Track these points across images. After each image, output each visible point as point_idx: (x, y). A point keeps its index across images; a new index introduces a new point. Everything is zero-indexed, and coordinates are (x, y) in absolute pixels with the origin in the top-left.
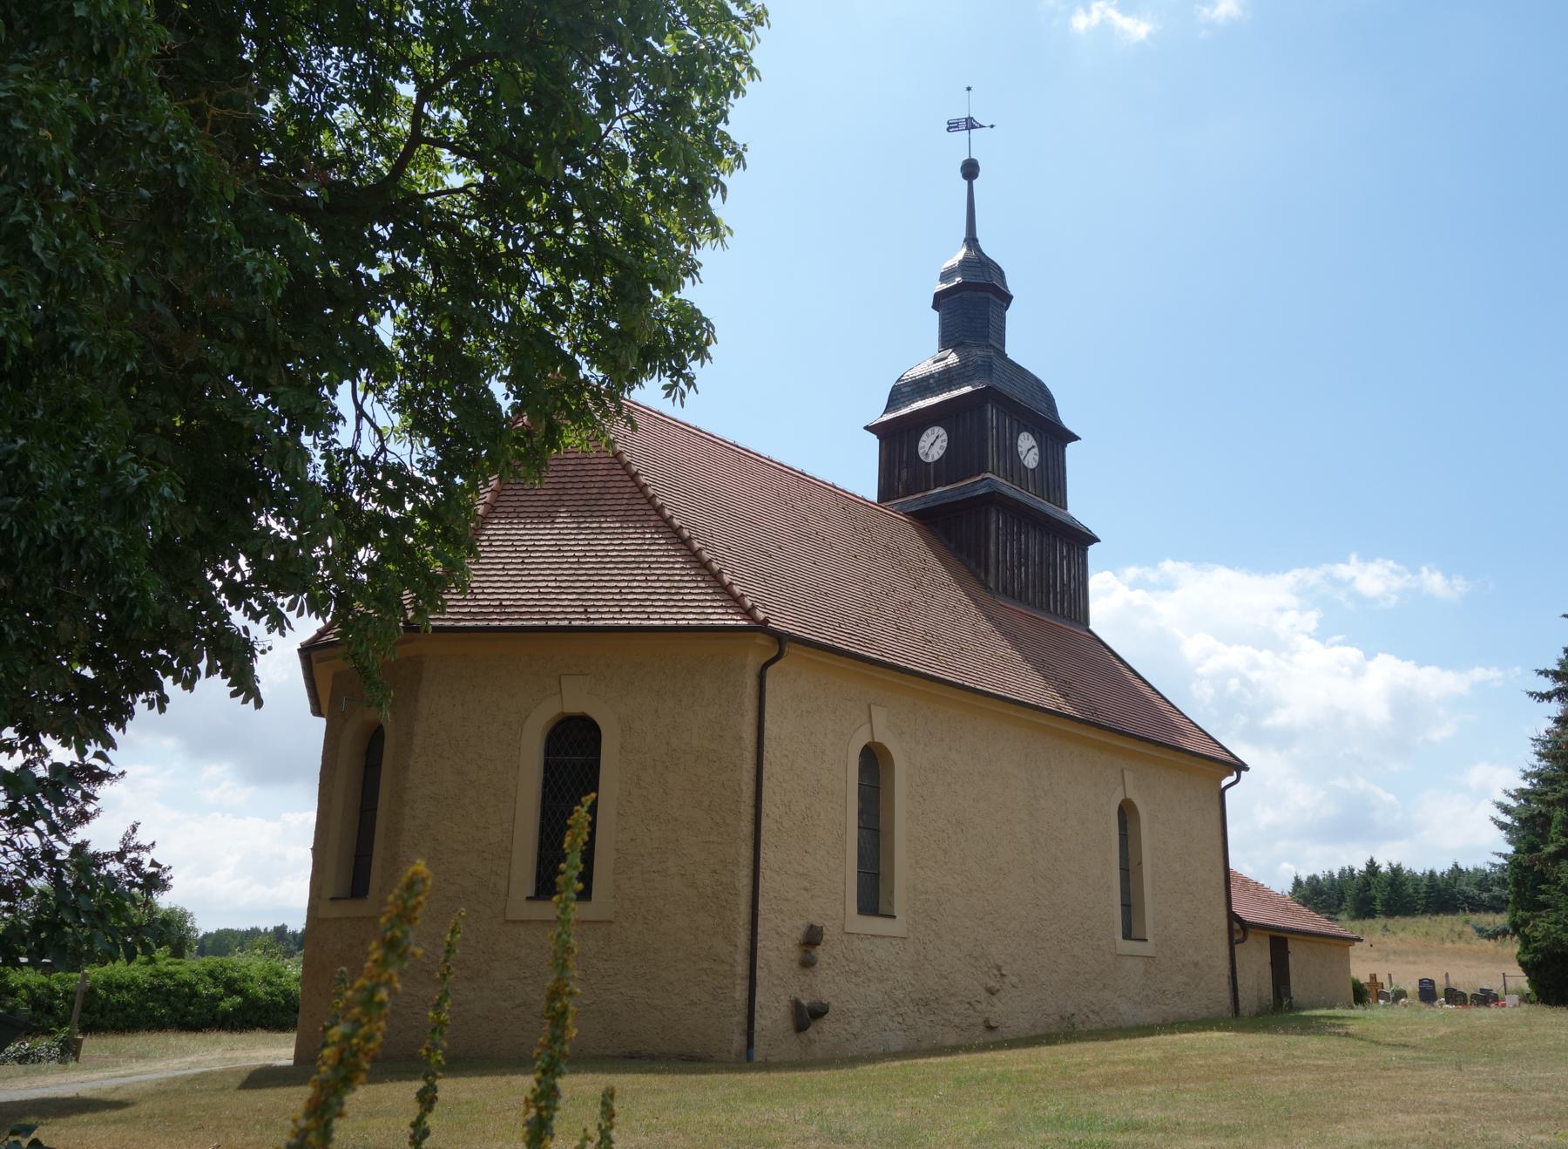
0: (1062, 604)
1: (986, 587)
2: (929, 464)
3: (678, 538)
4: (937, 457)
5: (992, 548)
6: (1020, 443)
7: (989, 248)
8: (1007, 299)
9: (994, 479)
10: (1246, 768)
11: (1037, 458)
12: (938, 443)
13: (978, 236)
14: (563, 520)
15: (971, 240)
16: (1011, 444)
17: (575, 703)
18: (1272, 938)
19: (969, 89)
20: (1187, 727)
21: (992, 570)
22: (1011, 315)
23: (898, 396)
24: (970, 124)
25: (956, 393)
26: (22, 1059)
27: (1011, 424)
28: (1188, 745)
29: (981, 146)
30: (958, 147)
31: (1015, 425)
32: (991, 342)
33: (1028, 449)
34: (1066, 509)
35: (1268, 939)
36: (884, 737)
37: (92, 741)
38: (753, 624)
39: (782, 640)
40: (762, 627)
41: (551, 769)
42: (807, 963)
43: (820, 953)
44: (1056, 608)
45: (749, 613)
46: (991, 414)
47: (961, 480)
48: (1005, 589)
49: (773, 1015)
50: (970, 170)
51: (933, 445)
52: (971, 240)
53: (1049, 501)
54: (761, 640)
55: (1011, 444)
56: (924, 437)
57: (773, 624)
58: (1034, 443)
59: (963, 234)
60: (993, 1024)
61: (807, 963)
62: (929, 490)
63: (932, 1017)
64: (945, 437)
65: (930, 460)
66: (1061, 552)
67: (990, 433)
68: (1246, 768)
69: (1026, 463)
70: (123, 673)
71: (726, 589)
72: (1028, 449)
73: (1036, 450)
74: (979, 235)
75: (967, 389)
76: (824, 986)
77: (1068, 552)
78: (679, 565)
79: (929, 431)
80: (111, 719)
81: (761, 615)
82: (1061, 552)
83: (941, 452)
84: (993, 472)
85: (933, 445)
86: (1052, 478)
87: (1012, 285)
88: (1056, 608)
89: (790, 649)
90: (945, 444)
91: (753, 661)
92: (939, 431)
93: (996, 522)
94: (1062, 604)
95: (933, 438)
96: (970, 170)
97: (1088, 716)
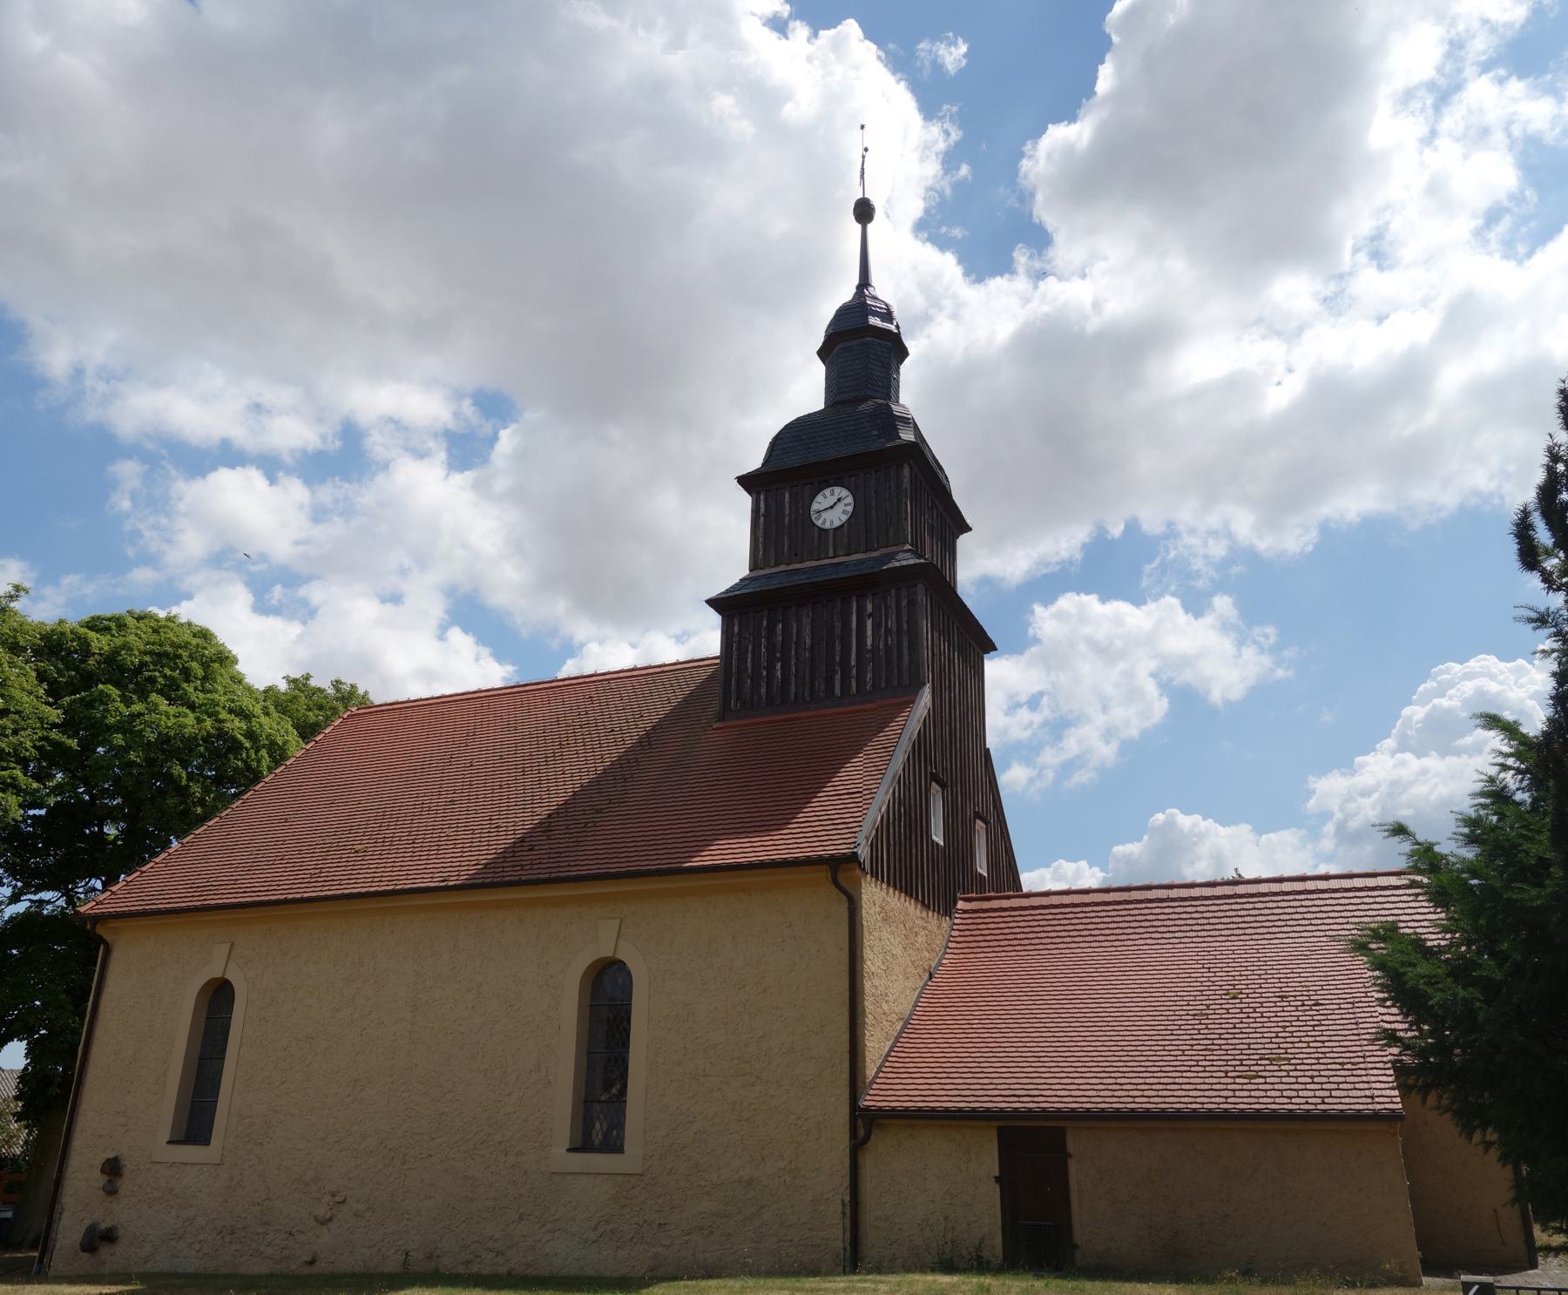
2: (826, 531)
12: (840, 507)
13: (854, 290)
18: (1000, 1129)
26: (1048, 564)
35: (994, 1134)
42: (111, 1191)
43: (124, 1185)
49: (68, 1232)
60: (309, 1259)
61: (111, 1191)
63: (238, 1247)
64: (850, 500)
70: (27, 650)
76: (122, 1213)
79: (827, 492)
80: (930, 235)
83: (845, 518)
90: (850, 509)
95: (833, 500)
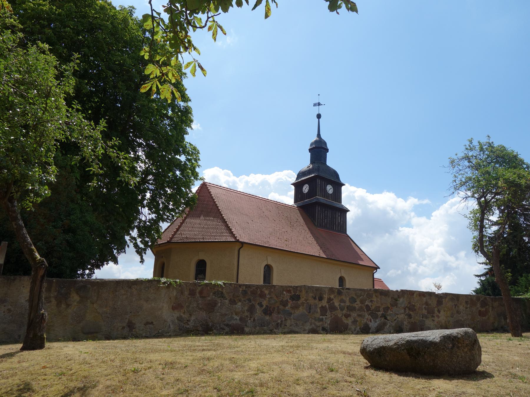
0: (338, 227)
1: (315, 225)
3: (224, 222)
4: (307, 192)
5: (317, 215)
6: (327, 187)
7: (323, 137)
8: (327, 150)
9: (320, 198)
10: (379, 268)
11: (332, 191)
13: (321, 134)
14: (202, 218)
15: (319, 135)
16: (325, 188)
17: (201, 258)
19: (319, 95)
20: (363, 257)
21: (316, 221)
22: (328, 154)
23: (300, 175)
24: (319, 104)
25: (311, 176)
27: (324, 184)
28: (361, 263)
29: (321, 110)
30: (316, 110)
31: (326, 183)
32: (322, 162)
33: (330, 189)
34: (341, 203)
36: (270, 262)
37: (155, 218)
38: (236, 240)
39: (243, 243)
40: (238, 241)
41: (197, 270)
44: (336, 228)
45: (235, 238)
46: (319, 181)
47: (312, 198)
48: (320, 225)
50: (319, 116)
51: (306, 189)
52: (319, 135)
53: (336, 201)
54: (238, 244)
55: (325, 188)
56: (304, 187)
57: (241, 240)
58: (332, 187)
59: (317, 133)
62: (305, 200)
64: (308, 187)
65: (305, 193)
66: (338, 214)
67: (318, 186)
68: (379, 268)
69: (329, 193)
71: (232, 233)
72: (330, 189)
73: (332, 189)
74: (321, 134)
75: (313, 175)
77: (340, 215)
78: (223, 227)
79: (305, 185)
81: (237, 238)
82: (338, 214)
84: (318, 196)
85: (306, 189)
86: (337, 195)
87: (329, 146)
88: (336, 228)
89: (245, 245)
91: (237, 248)
92: (307, 185)
93: (318, 209)
94: (338, 227)
96: (319, 116)
97: (329, 257)
